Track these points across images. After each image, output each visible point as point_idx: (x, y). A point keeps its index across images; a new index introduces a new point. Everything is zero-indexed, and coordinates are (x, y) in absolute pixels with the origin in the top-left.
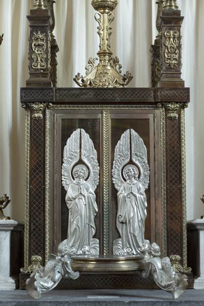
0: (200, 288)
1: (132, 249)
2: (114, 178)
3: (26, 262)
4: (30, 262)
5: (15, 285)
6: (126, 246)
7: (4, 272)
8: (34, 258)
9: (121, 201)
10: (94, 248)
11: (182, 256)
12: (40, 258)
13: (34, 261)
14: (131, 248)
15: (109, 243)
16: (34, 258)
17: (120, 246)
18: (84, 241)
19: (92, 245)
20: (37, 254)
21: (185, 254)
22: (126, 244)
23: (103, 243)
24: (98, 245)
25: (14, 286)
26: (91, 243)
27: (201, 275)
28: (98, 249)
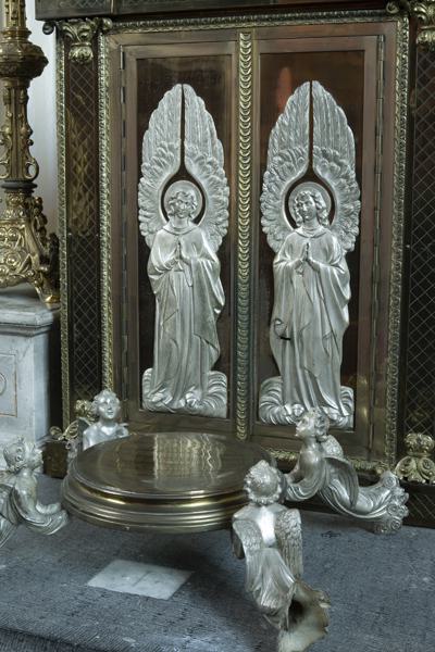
6: (293, 398)
14: (304, 405)
23: (235, 386)
24: (224, 390)
26: (207, 383)
28: (225, 401)
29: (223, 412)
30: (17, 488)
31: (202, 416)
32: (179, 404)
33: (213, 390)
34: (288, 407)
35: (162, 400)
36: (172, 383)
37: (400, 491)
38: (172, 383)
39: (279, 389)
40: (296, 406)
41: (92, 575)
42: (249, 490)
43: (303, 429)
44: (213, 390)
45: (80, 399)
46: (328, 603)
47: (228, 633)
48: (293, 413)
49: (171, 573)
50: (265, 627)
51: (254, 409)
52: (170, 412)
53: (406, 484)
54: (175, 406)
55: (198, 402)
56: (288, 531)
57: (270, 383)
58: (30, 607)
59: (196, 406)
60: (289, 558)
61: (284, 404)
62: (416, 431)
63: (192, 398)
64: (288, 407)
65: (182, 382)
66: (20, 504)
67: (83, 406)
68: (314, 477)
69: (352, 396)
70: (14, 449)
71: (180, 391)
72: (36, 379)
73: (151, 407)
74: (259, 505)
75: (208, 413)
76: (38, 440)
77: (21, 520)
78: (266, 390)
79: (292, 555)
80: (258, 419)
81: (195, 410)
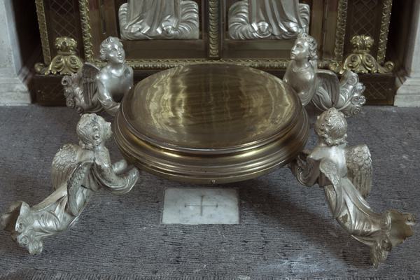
0: (407, 104)
1: (270, 25)
2: (246, 6)
3: (45, 42)
4: (54, 51)
5: (28, 96)
6: (258, 17)
7: (5, 66)
8: (60, 42)
9: (285, 93)
10: (187, 22)
11: (376, 37)
12: (72, 42)
13: (61, 49)
14: (267, 21)
15: (219, 18)
16: (60, 42)
17: (244, 18)
18: (165, 9)
19: (183, 15)
20: (64, 34)
21: (384, 33)
22: (258, 14)
23: (207, 12)
24: (196, 16)
25: (29, 101)
26: (181, 11)
27: (412, 75)
28: (197, 24)
29: (196, 34)
30: (97, 162)
31: (177, 39)
32: (157, 32)
33: (186, 16)
34: (254, 25)
35: (140, 30)
36: (148, 14)
37: (360, 86)
38: (148, 14)
39: (245, 11)
40: (261, 24)
41: (159, 213)
42: (326, 136)
43: (298, 52)
44: (186, 16)
45: (59, 36)
46: (414, 221)
47: (312, 248)
48: (259, 29)
49: (220, 194)
50: (334, 235)
51: (224, 27)
52: (148, 39)
53: (362, 78)
54: (153, 34)
55: (173, 28)
56: (361, 164)
57: (238, 6)
58: (135, 261)
59: (173, 32)
60: (360, 183)
61: (250, 23)
62: (360, 34)
63: (170, 25)
64: (254, 25)
65: (158, 14)
66: (103, 176)
67: (64, 43)
68: (310, 91)
69: (308, 10)
70: (90, 129)
71: (156, 20)
72: (8, 22)
73: (129, 37)
74: (330, 146)
75: (183, 36)
76: (18, 74)
77: (102, 186)
78: (233, 13)
79: (363, 181)
80: (228, 36)
81: (172, 35)
